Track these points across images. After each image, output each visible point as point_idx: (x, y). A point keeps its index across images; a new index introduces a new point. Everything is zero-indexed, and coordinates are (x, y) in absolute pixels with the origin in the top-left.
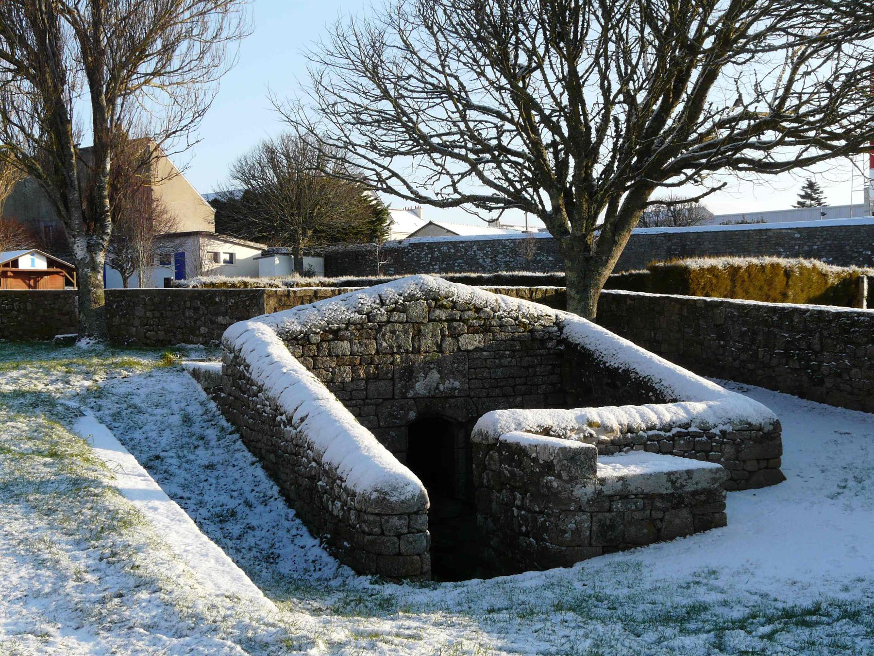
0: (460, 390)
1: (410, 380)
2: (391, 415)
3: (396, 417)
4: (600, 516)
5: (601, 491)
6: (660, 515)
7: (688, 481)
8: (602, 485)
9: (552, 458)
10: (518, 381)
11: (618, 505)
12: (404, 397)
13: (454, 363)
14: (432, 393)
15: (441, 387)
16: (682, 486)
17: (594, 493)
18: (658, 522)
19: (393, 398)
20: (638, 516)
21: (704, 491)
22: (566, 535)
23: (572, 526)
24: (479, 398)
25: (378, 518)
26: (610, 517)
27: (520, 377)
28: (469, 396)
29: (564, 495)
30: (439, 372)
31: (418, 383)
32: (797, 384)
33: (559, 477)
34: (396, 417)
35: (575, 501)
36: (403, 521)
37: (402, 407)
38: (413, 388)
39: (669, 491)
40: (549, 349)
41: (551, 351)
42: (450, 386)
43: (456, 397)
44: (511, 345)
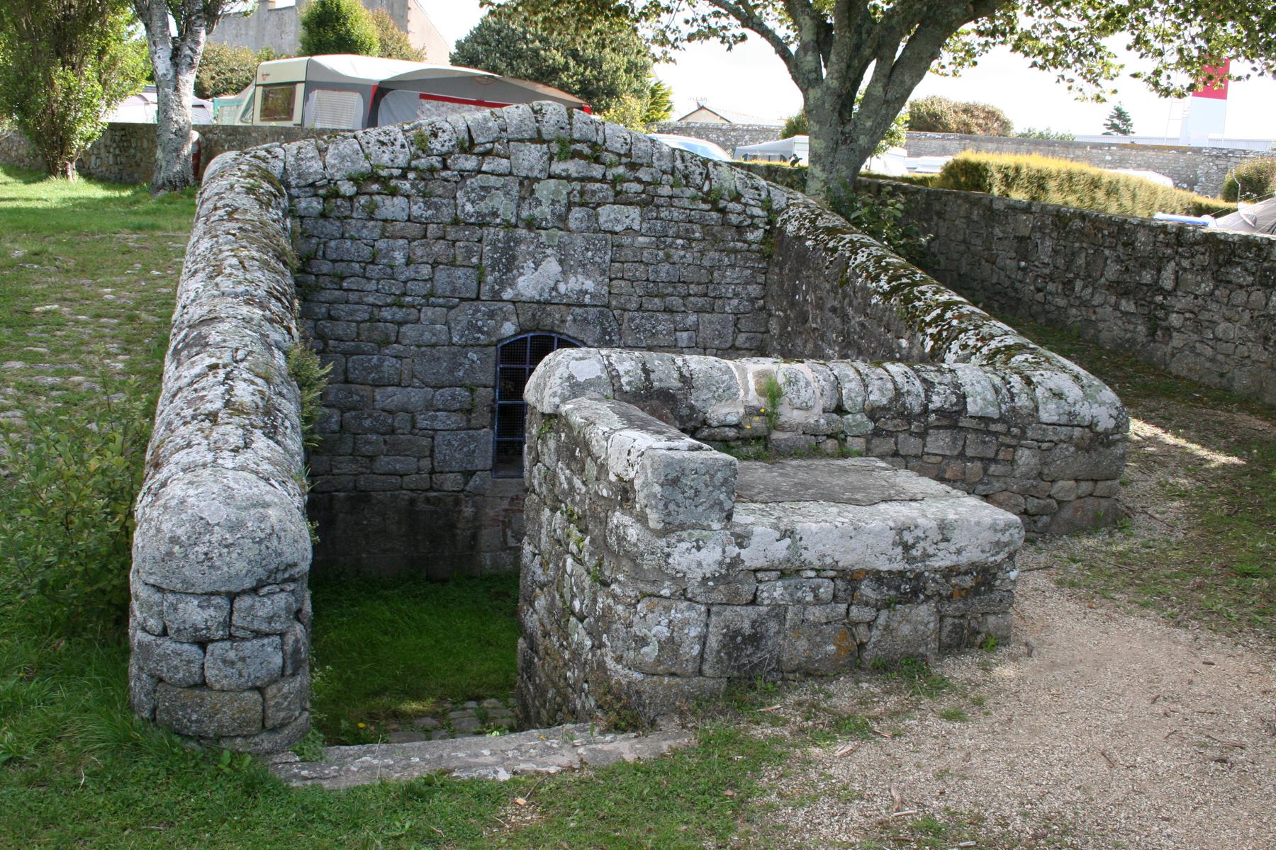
0: (593, 296)
1: (509, 270)
2: (471, 326)
3: (480, 330)
4: (728, 613)
5: (737, 561)
6: (866, 614)
7: (943, 545)
8: (741, 546)
9: (632, 474)
10: (694, 289)
11: (776, 591)
12: (496, 297)
13: (587, 250)
14: (546, 296)
15: (562, 288)
16: (926, 556)
17: (720, 564)
18: (862, 629)
19: (478, 298)
20: (815, 614)
21: (973, 568)
22: (645, 649)
23: (664, 631)
24: (625, 310)
25: (157, 597)
26: (754, 616)
27: (698, 284)
28: (608, 306)
29: (648, 563)
30: (561, 262)
31: (521, 279)
32: (1129, 335)
33: (642, 519)
34: (480, 330)
35: (673, 578)
36: (212, 611)
37: (491, 315)
38: (512, 284)
39: (898, 566)
40: (750, 243)
41: (754, 247)
42: (577, 287)
43: (585, 306)
44: (687, 230)
